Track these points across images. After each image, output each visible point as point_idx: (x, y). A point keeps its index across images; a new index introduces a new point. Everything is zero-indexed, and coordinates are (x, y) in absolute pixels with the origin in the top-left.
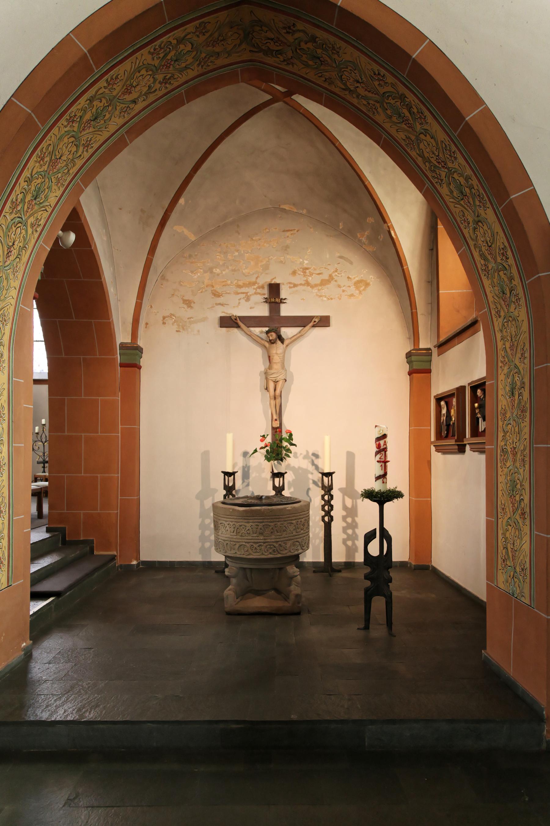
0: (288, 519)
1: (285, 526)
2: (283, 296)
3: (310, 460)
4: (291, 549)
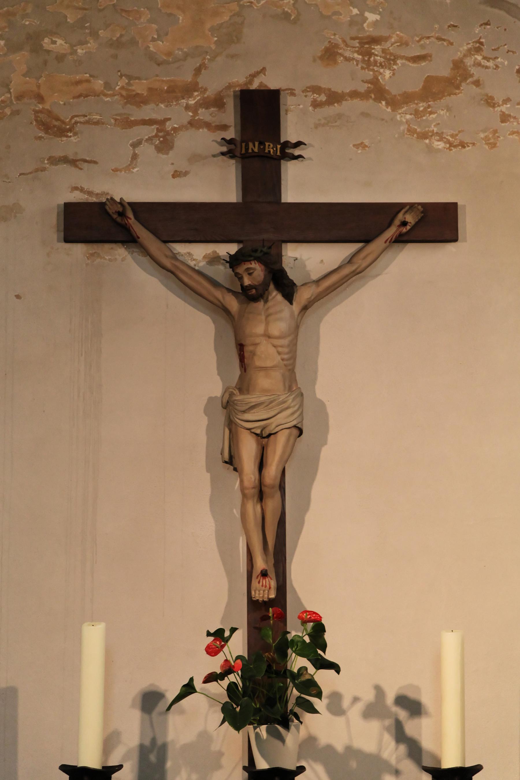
3: (388, 722)
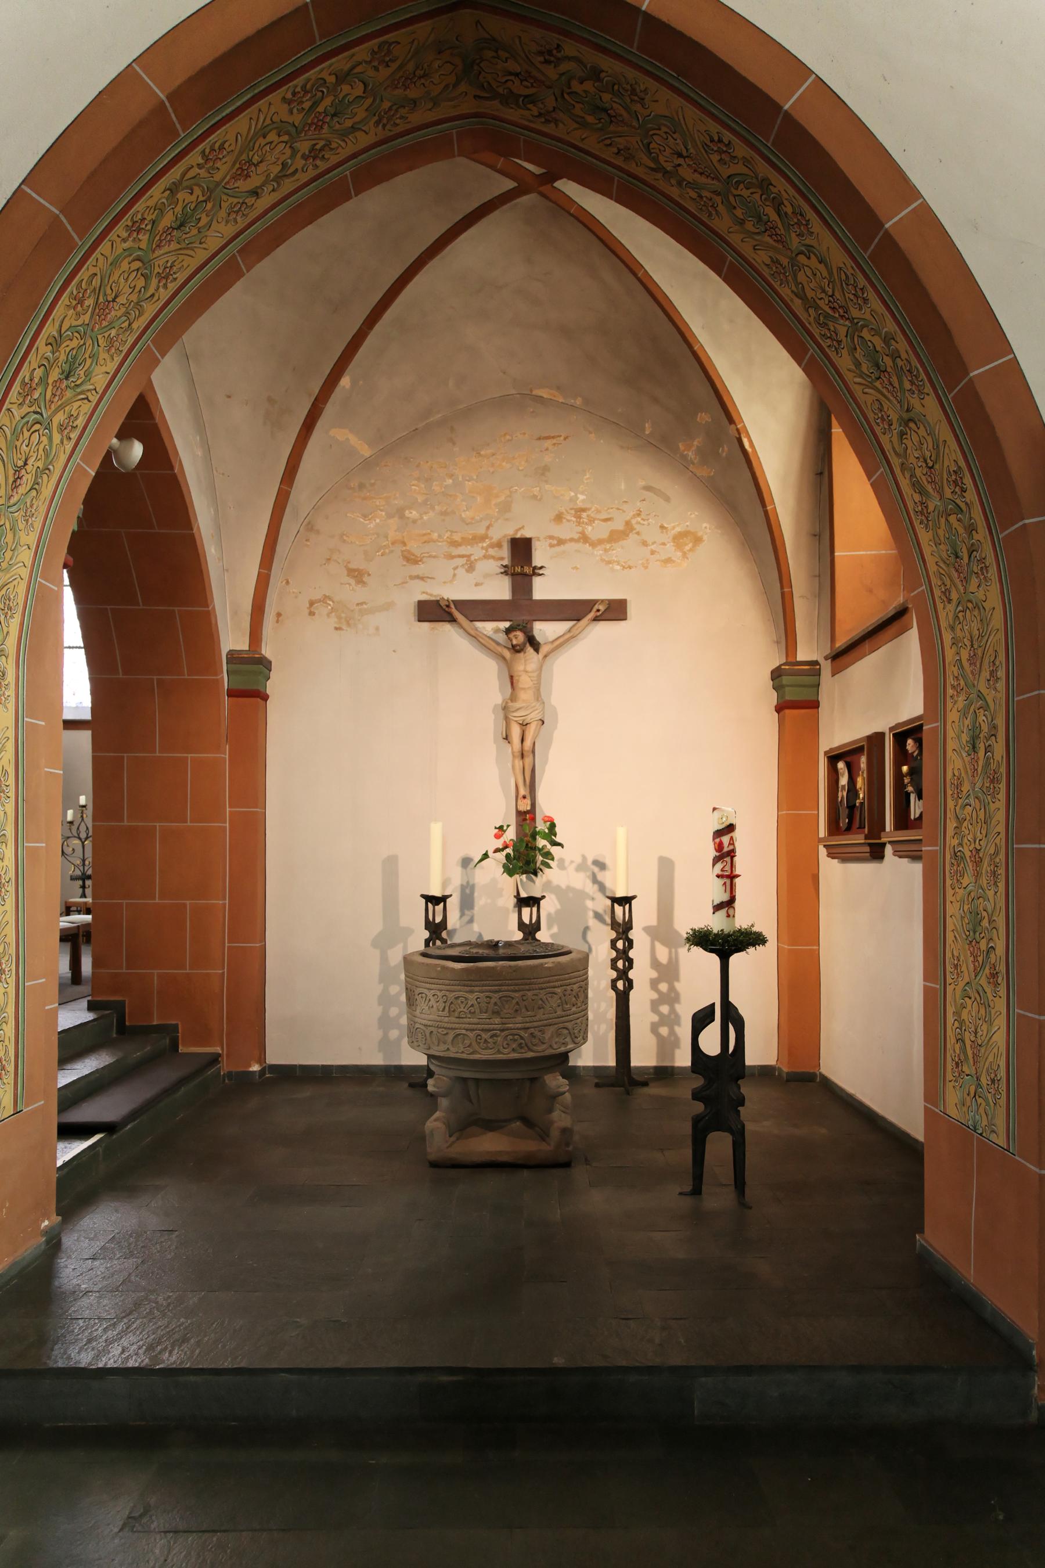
0: (548, 985)
1: (541, 999)
2: (537, 561)
3: (589, 873)
4: (554, 1043)
